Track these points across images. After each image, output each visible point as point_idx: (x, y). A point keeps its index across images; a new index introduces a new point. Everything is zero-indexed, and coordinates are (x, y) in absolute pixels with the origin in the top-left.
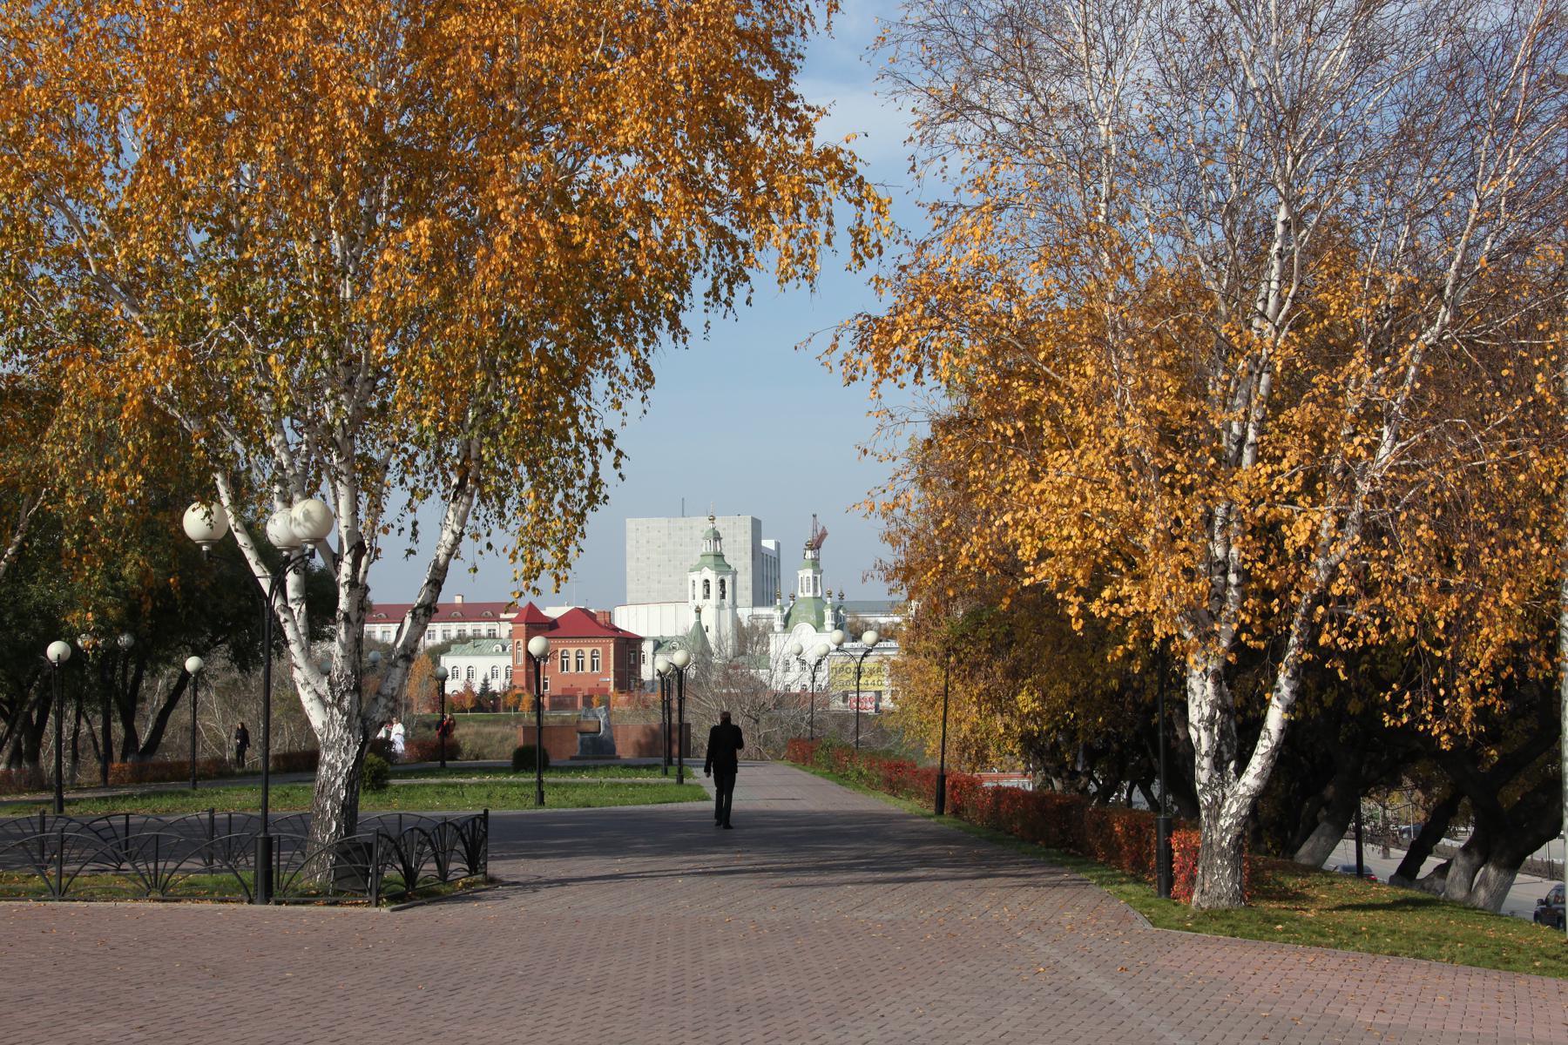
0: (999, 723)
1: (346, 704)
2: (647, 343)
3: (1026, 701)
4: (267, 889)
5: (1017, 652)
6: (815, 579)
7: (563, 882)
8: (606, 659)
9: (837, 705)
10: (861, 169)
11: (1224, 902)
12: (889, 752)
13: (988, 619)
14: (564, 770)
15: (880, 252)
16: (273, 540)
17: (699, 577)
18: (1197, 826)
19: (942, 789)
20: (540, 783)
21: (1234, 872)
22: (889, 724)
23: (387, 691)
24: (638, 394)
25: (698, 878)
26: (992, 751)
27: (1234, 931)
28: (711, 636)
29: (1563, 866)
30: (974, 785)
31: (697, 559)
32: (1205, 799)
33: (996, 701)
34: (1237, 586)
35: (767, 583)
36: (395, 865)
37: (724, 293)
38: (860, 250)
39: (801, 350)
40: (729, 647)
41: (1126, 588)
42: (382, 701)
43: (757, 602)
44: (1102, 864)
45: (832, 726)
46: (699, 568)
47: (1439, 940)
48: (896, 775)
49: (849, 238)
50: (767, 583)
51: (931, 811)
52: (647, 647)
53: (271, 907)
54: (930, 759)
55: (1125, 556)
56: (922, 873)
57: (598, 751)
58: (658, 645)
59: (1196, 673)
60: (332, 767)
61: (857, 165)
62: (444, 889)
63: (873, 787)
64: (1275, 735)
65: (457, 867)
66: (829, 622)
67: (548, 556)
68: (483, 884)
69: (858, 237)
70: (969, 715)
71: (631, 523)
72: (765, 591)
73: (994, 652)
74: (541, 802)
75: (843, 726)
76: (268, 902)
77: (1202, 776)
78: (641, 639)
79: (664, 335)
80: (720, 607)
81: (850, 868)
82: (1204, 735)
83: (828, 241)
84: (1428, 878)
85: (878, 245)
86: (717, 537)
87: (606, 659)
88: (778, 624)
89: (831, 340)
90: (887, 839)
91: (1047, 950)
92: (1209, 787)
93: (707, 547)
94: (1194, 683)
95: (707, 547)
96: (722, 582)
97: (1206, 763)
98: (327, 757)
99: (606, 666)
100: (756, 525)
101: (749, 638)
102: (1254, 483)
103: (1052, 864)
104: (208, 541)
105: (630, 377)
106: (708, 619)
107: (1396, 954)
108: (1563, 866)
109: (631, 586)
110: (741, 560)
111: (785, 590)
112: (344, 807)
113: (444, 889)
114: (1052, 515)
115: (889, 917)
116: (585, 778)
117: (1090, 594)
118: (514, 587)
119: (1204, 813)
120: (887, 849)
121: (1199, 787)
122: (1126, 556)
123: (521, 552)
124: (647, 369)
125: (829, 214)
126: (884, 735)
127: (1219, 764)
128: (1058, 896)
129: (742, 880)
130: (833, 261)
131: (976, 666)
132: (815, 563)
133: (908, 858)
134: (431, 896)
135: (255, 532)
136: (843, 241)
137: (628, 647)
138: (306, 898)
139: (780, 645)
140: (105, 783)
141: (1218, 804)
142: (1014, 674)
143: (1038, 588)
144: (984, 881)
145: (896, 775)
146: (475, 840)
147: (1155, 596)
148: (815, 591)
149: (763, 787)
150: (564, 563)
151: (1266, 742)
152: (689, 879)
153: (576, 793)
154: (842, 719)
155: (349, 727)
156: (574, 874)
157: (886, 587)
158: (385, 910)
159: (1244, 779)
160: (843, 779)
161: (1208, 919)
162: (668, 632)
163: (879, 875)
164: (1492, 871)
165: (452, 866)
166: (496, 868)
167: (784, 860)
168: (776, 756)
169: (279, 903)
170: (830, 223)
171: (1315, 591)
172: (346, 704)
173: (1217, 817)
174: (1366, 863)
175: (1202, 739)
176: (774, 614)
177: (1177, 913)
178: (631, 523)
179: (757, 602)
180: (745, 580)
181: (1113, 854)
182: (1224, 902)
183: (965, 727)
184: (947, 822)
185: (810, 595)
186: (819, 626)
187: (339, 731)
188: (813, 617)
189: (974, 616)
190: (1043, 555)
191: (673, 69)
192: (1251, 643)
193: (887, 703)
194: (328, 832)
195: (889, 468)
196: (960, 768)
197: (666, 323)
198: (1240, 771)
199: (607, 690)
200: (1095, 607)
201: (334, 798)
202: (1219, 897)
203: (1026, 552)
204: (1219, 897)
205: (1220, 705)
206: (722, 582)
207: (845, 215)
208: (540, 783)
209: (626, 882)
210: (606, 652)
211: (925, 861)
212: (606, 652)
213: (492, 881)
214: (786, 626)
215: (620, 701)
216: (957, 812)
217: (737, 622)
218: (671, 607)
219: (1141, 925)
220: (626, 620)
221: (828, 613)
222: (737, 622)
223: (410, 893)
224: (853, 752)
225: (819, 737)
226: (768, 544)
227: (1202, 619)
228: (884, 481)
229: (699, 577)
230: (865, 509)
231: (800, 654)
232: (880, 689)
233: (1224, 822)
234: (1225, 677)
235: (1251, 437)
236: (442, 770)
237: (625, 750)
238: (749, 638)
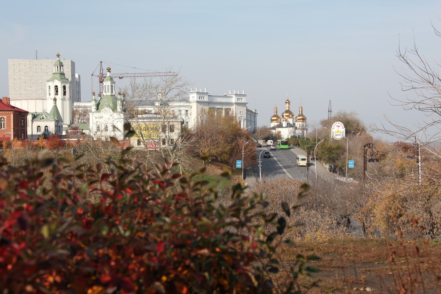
2: (319, 140)
6: (112, 86)
8: (9, 122)
29: (210, 107)
31: (51, 76)
46: (53, 80)
52: (29, 117)
58: (34, 117)
66: (119, 108)
78: (27, 113)
80: (63, 100)
87: (9, 122)
88: (94, 109)
93: (55, 70)
96: (64, 87)
99: (9, 126)
102: (341, 250)
108: (210, 107)
137: (20, 116)
148: (112, 92)
162: (39, 111)
171: (251, 251)
174: (303, 113)
185: (109, 94)
188: (111, 105)
199: (9, 138)
206: (64, 87)
210: (9, 119)
212: (9, 119)
214: (97, 109)
215: (17, 145)
218: (41, 101)
221: (119, 103)
229: (52, 85)
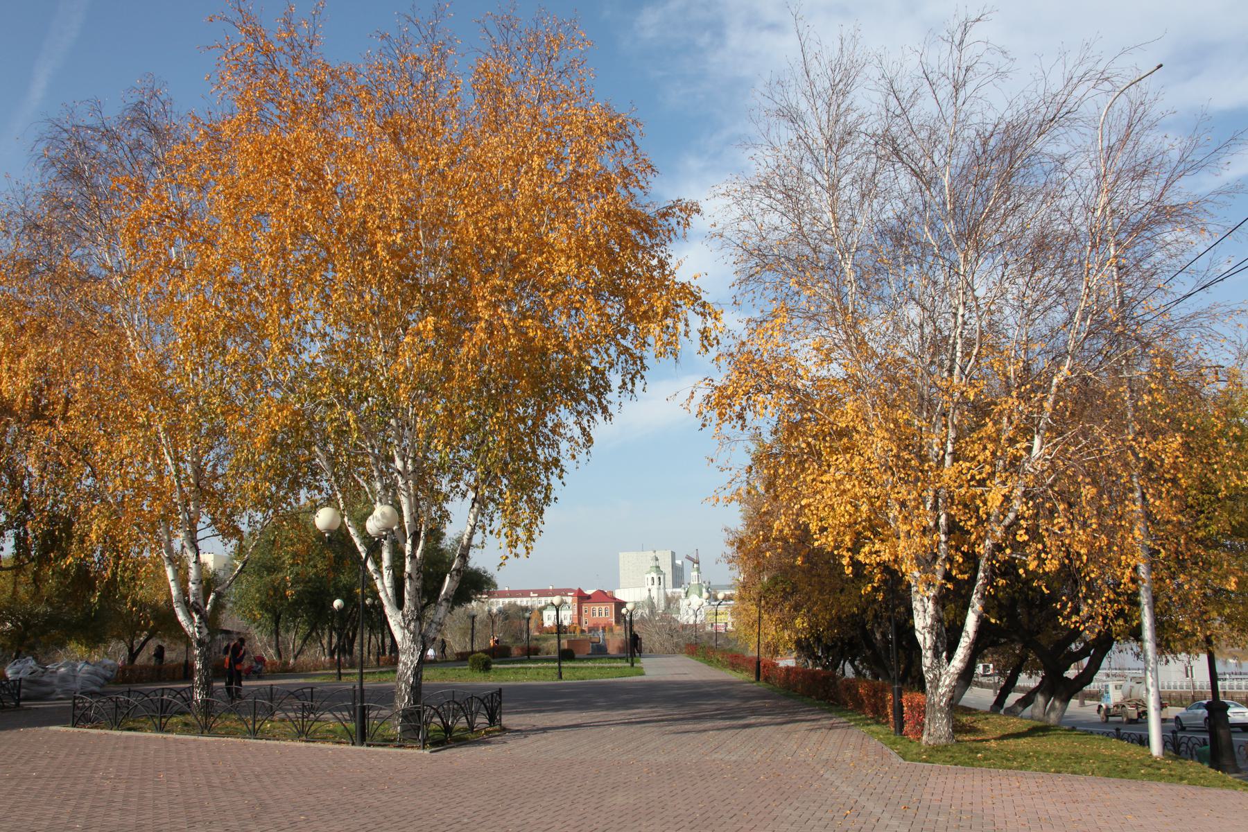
0: (786, 634)
1: (412, 627)
3: (798, 623)
4: (363, 736)
5: (797, 597)
7: (545, 730)
9: (709, 628)
10: (705, 298)
11: (943, 740)
12: (731, 650)
13: (790, 569)
14: (581, 660)
15: (718, 343)
16: (369, 531)
17: (649, 576)
18: (922, 689)
19: (760, 669)
20: (560, 667)
21: (948, 721)
22: (731, 636)
23: (437, 620)
24: (585, 450)
25: (623, 727)
26: (781, 648)
27: (953, 760)
28: (655, 601)
30: (775, 665)
32: (929, 676)
33: (785, 624)
34: (946, 542)
35: (678, 579)
36: (443, 722)
37: (629, 386)
38: (706, 343)
39: (671, 401)
40: (662, 605)
41: (877, 546)
42: (434, 626)
43: (674, 586)
44: (851, 710)
45: (705, 638)
47: (1078, 758)
48: (735, 661)
49: (699, 335)
50: (678, 579)
51: (753, 679)
53: (364, 748)
54: (752, 652)
55: (876, 527)
56: (752, 720)
57: (600, 651)
59: (918, 597)
60: (405, 664)
61: (702, 294)
62: (470, 736)
63: (724, 666)
64: (972, 635)
65: (481, 720)
67: (520, 532)
68: (497, 730)
69: (704, 334)
70: (771, 631)
71: (621, 555)
72: (678, 582)
73: (785, 598)
74: (561, 677)
75: (710, 638)
76: (362, 744)
77: (927, 661)
79: (599, 417)
81: (712, 717)
82: (928, 636)
83: (686, 334)
84: (1013, 706)
85: (716, 338)
86: (657, 559)
88: (683, 595)
89: (689, 394)
90: (732, 697)
91: (844, 787)
92: (931, 669)
93: (653, 563)
94: (916, 605)
95: (653, 563)
97: (929, 654)
98: (403, 658)
100: (673, 554)
101: (670, 601)
103: (823, 711)
104: (329, 531)
105: (581, 441)
106: (654, 593)
107: (1060, 772)
109: (622, 580)
110: (667, 569)
111: (686, 582)
112: (412, 688)
113: (470, 736)
114: (828, 506)
115: (734, 758)
116: (590, 664)
117: (855, 549)
118: (501, 553)
119: (928, 685)
120: (733, 703)
121: (924, 669)
122: (876, 527)
123: (504, 531)
124: (589, 435)
125: (686, 320)
126: (728, 641)
127: (937, 655)
128: (836, 735)
129: (648, 728)
130: (690, 345)
131: (776, 605)
132: (698, 569)
133: (744, 709)
134: (461, 742)
135: (362, 530)
136: (695, 336)
137: (620, 604)
138: (386, 742)
139: (683, 603)
140: (378, 665)
141: (937, 679)
142: (797, 608)
143: (821, 549)
144: (789, 726)
145: (735, 661)
146: (494, 704)
147: (903, 549)
149: (657, 669)
150: (530, 538)
151: (966, 639)
152: (619, 728)
153: (579, 673)
154: (710, 635)
155: (414, 641)
156: (555, 724)
157: (728, 566)
158: (426, 752)
159: (953, 663)
160: (710, 663)
161: (934, 753)
163: (728, 723)
164: (1057, 704)
165: (478, 720)
166: (507, 720)
167: (676, 713)
168: (681, 652)
169: (369, 745)
170: (687, 325)
172: (412, 627)
173: (937, 687)
175: (925, 638)
176: (681, 591)
177: (914, 749)
178: (621, 555)
179: (674, 586)
180: (669, 577)
181: (859, 706)
182: (943, 740)
183: (770, 637)
184: (762, 686)
186: (700, 595)
187: (408, 643)
189: (774, 580)
190: (823, 529)
191: (588, 229)
192: (959, 576)
193: (730, 627)
194: (403, 702)
195: (727, 476)
196: (766, 657)
197: (600, 411)
198: (949, 659)
200: (861, 558)
201: (407, 682)
202: (940, 737)
203: (813, 527)
204: (940, 737)
205: (938, 619)
207: (696, 323)
208: (560, 667)
209: (581, 730)
211: (754, 712)
213: (504, 730)
216: (767, 679)
217: (666, 595)
219: (896, 760)
220: (620, 595)
222: (666, 595)
223: (445, 739)
224: (714, 650)
225: (698, 644)
226: (678, 562)
227: (926, 561)
228: (724, 483)
229: (649, 576)
230: (713, 501)
231: (692, 609)
232: (726, 621)
233: (942, 690)
234: (941, 600)
235: (950, 449)
236: (530, 660)
237: (612, 649)
238: (670, 601)
